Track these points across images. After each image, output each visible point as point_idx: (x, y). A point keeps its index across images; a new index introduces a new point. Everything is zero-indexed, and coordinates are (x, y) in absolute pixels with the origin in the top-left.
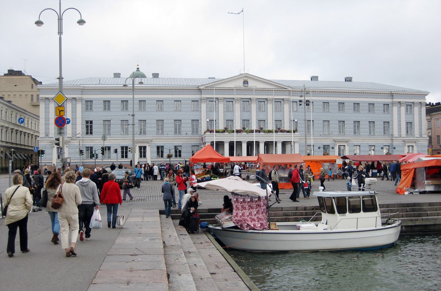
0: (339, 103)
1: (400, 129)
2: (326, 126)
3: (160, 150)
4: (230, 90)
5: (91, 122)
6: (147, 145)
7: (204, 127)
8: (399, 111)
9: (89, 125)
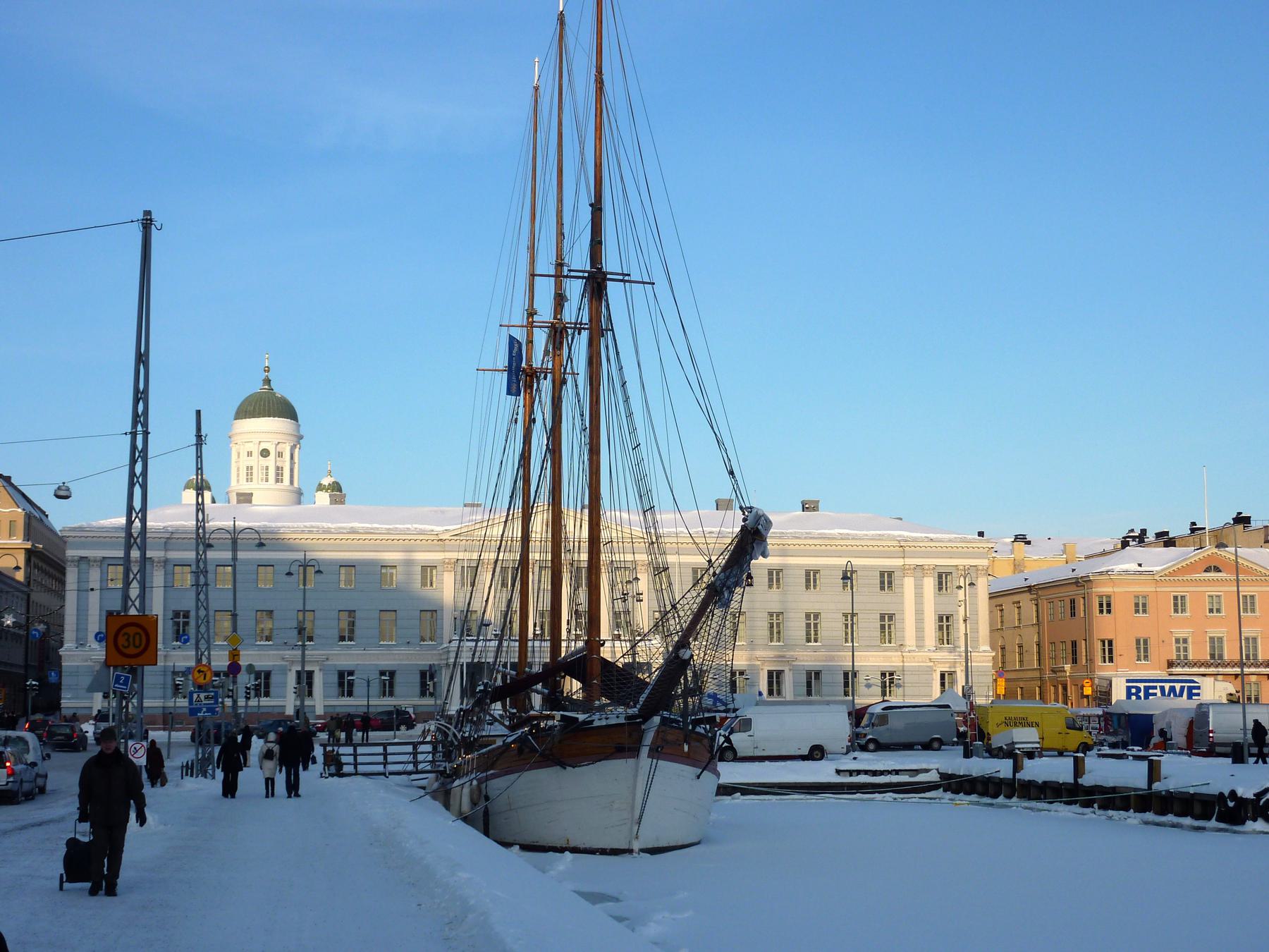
1: (920, 630)
3: (345, 682)
5: (817, 616)
6: (786, 669)
9: (945, 623)
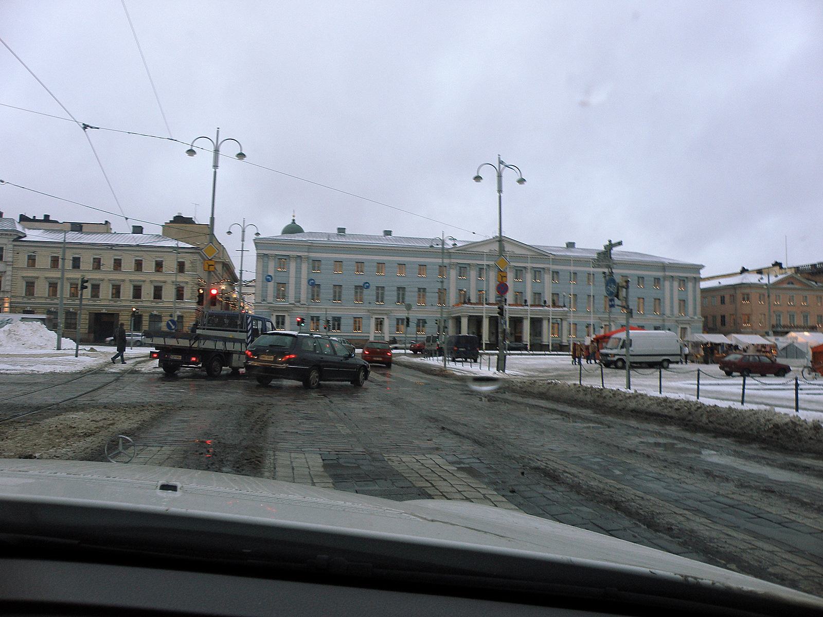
1: (672, 307)
2: (641, 305)
6: (385, 317)
8: (672, 286)
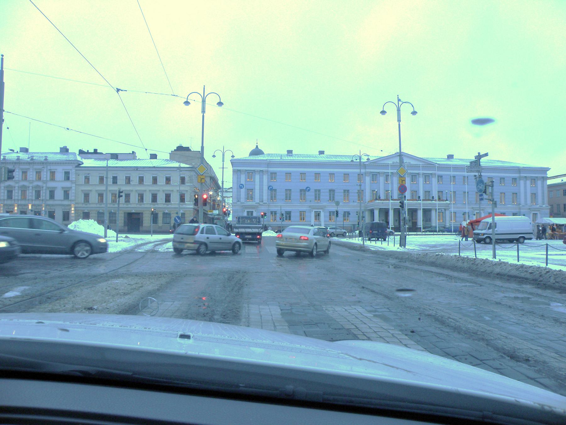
0: (501, 178)
4: (387, 166)
6: (254, 211)
7: (368, 196)
8: (525, 184)
